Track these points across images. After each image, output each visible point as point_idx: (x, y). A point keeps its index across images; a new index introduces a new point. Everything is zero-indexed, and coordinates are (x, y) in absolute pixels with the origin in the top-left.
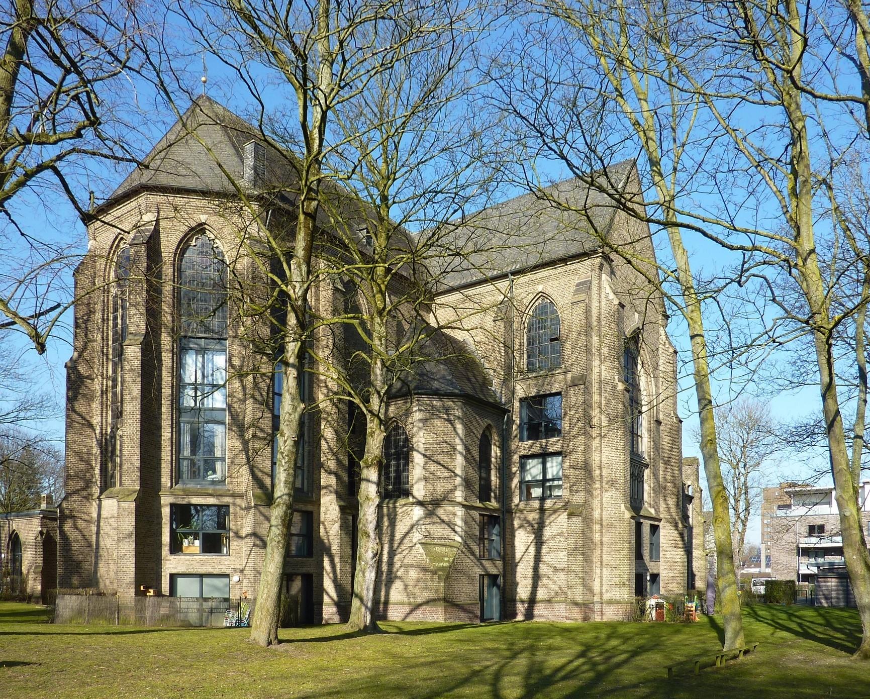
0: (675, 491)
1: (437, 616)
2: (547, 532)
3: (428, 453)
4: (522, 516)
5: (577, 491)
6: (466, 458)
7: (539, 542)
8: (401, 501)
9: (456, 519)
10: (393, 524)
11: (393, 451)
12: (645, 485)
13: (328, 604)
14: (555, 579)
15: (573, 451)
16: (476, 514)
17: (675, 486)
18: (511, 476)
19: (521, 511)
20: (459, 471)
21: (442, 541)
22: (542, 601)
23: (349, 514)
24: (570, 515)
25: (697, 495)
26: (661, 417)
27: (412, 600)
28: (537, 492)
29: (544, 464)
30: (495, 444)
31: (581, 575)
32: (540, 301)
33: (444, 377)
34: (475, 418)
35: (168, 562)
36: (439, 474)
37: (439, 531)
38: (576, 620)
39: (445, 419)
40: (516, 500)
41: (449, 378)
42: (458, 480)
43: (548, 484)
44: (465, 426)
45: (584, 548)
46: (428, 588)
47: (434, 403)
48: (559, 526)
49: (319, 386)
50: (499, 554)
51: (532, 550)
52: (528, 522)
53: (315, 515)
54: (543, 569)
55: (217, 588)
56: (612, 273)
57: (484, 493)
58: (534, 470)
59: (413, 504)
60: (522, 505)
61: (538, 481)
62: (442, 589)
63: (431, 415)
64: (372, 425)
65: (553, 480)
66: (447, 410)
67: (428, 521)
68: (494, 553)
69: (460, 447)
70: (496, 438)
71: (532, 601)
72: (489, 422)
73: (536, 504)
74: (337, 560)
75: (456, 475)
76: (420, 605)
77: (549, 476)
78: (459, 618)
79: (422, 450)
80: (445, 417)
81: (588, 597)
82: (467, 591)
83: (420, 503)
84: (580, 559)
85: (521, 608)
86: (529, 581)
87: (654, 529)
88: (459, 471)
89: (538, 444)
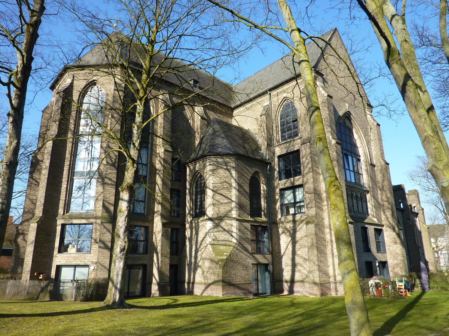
0: (390, 206)
1: (217, 292)
2: (299, 235)
3: (215, 189)
4: (284, 226)
5: (311, 208)
6: (238, 191)
7: (294, 242)
8: (201, 219)
9: (233, 228)
10: (197, 233)
11: (199, 190)
12: (368, 204)
13: (154, 284)
14: (305, 266)
15: (307, 182)
16: (248, 225)
17: (389, 203)
18: (275, 202)
19: (282, 223)
20: (234, 199)
21: (224, 243)
22: (298, 281)
23: (168, 227)
24: (307, 223)
25: (420, 212)
26: (374, 162)
27: (206, 281)
28: (292, 211)
29: (294, 193)
30: (263, 183)
31: (317, 263)
32: (286, 102)
33: (225, 146)
34: (245, 167)
35: (56, 258)
36: (222, 201)
37: (223, 236)
38: (316, 295)
39: (225, 169)
40: (279, 216)
41: (229, 146)
42: (234, 205)
43: (297, 205)
44: (238, 172)
45: (319, 246)
46: (214, 273)
47: (219, 160)
48: (303, 231)
49: (156, 156)
50: (269, 250)
51: (290, 247)
52: (287, 229)
53: (150, 228)
54: (298, 260)
55: (83, 274)
56: (324, 81)
57: (255, 211)
58: (289, 197)
59: (206, 220)
60: (283, 219)
61: (291, 203)
62: (221, 274)
63: (218, 166)
64: (129, 164)
65: (300, 202)
66: (226, 164)
67: (216, 230)
68: (266, 250)
69: (234, 185)
70: (263, 179)
71: (292, 281)
72: (257, 170)
73: (290, 218)
74: (160, 255)
75: (232, 201)
76: (210, 285)
77: (298, 200)
78: (235, 294)
79: (212, 188)
80: (225, 167)
81: (324, 278)
82: (244, 274)
83: (210, 219)
84: (315, 252)
85: (286, 286)
86: (290, 268)
87: (379, 232)
88: (234, 199)
89: (289, 181)
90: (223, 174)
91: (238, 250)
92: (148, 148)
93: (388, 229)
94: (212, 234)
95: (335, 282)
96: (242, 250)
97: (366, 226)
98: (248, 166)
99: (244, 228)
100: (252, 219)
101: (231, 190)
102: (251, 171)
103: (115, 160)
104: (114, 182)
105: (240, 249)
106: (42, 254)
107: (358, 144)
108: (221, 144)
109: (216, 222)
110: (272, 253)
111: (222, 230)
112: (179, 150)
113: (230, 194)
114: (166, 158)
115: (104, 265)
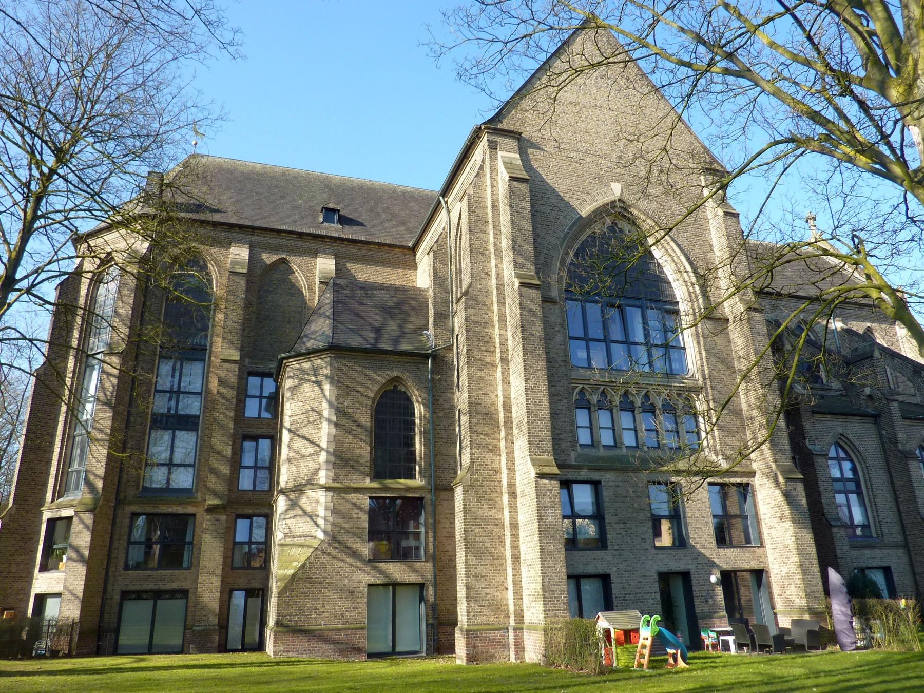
20: (324, 444)
21: (301, 540)
36: (304, 451)
39: (313, 382)
42: (323, 456)
66: (316, 371)
67: (291, 513)
75: (322, 449)
80: (313, 379)
88: (324, 444)
90: (308, 394)
91: (329, 554)
92: (204, 360)
93: (765, 481)
94: (284, 522)
95: (519, 626)
96: (339, 556)
98: (371, 368)
99: (350, 506)
100: (375, 485)
102: (380, 379)
103: (112, 393)
104: (106, 434)
105: (334, 552)
106: (11, 575)
107: (669, 271)
108: (316, 332)
109: (292, 496)
110: (434, 559)
111: (300, 512)
114: (223, 375)
115: (74, 592)
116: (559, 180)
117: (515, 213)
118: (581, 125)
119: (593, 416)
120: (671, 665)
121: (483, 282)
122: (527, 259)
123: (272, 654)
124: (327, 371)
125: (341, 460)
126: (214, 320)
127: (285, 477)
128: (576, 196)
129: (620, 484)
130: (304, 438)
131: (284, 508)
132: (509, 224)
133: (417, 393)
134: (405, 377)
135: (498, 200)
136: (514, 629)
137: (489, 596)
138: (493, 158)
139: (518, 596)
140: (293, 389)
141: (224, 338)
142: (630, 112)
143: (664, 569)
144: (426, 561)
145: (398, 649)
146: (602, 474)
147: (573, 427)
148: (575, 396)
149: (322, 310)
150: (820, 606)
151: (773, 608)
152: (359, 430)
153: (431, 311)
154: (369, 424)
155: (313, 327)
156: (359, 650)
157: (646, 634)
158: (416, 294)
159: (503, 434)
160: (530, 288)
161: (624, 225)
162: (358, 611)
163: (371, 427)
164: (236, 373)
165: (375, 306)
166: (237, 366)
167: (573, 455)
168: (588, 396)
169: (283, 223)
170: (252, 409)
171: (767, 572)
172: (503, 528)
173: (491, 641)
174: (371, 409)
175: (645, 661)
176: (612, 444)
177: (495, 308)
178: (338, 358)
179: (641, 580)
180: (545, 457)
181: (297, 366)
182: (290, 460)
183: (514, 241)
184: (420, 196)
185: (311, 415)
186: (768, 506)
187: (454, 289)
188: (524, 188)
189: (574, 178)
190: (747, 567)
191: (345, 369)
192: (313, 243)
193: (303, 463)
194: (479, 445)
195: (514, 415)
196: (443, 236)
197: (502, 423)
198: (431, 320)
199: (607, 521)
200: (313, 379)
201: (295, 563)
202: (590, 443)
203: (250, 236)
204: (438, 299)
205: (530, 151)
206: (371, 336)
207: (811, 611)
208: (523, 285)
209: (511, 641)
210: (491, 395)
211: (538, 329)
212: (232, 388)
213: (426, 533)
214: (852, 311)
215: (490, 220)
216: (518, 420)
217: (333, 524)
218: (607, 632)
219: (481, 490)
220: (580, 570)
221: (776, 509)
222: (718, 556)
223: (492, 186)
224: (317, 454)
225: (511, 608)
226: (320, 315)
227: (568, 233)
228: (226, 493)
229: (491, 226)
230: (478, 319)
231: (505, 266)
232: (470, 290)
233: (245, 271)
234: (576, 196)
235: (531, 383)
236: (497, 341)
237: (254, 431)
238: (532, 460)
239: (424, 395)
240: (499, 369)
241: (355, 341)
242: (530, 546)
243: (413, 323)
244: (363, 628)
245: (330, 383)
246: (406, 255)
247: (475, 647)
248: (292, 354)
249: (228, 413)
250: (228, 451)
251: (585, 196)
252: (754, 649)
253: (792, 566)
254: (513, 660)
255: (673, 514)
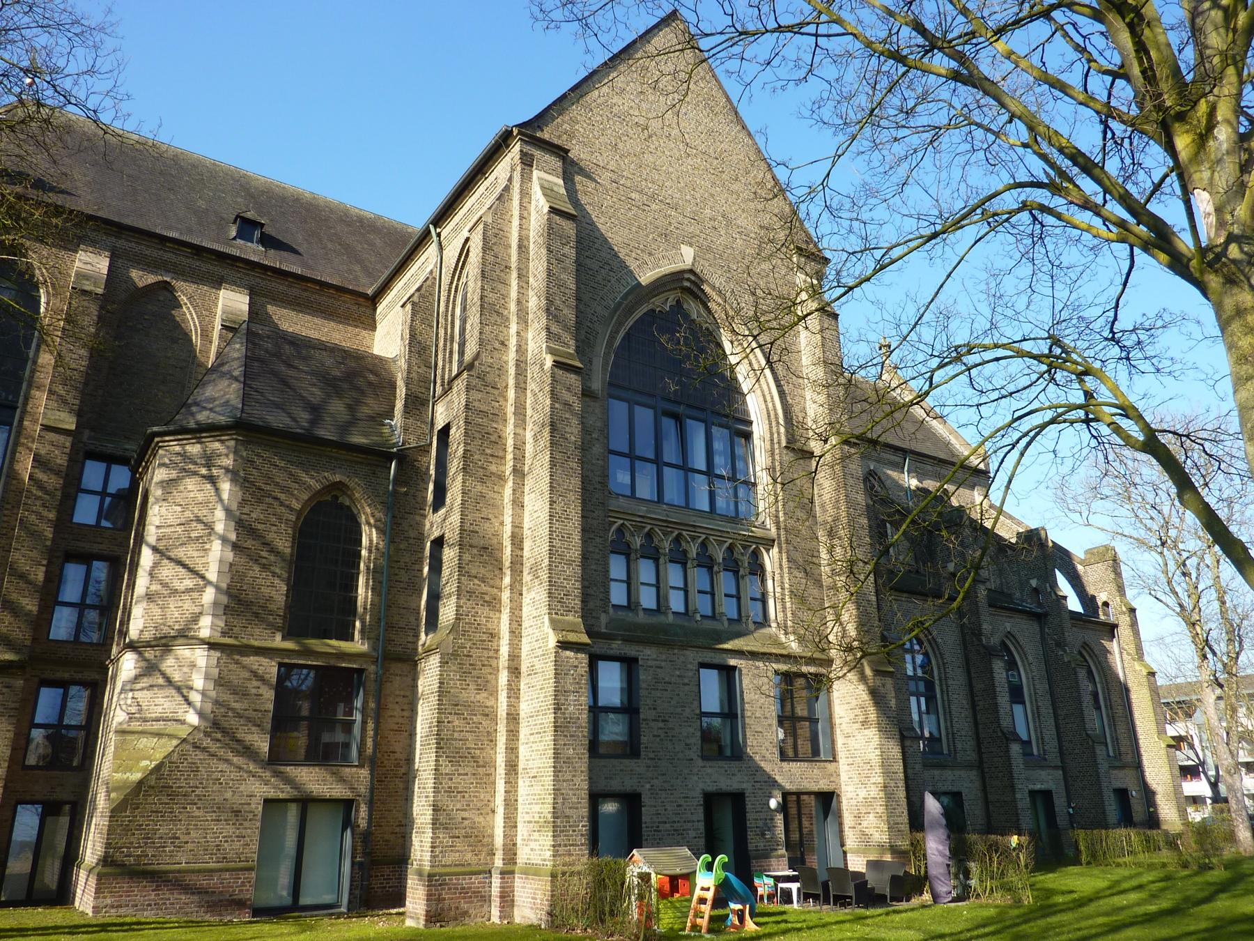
3: (161, 546)
9: (194, 676)
20: (212, 576)
21: (157, 726)
25: (1124, 621)
39: (203, 476)
42: (209, 595)
67: (145, 682)
75: (210, 583)
80: (204, 471)
88: (212, 576)
90: (192, 495)
91: (204, 749)
92: (11, 425)
94: (130, 694)
95: (509, 868)
96: (221, 753)
97: (732, 662)
98: (301, 465)
99: (247, 675)
100: (289, 645)
101: (207, 546)
102: (312, 482)
105: (214, 747)
108: (214, 399)
109: (149, 654)
110: (373, 763)
111: (161, 681)
112: (623, 478)
113: (204, 560)
114: (43, 452)
116: (615, 230)
117: (553, 261)
118: (649, 158)
119: (632, 566)
120: (733, 926)
121: (496, 355)
122: (566, 328)
123: (90, 912)
124: (228, 462)
125: (238, 603)
126: (35, 362)
127: (139, 623)
128: (634, 255)
129: (663, 664)
130: (179, 563)
131: (133, 673)
132: (544, 276)
133: (368, 510)
134: (352, 485)
135: (528, 238)
136: (501, 873)
137: (466, 822)
138: (526, 178)
139: (511, 823)
140: (168, 485)
141: (51, 392)
142: (712, 154)
143: (712, 788)
144: (361, 766)
145: (305, 900)
146: (641, 648)
147: (606, 580)
148: (611, 535)
149: (226, 368)
150: (904, 844)
151: (843, 845)
152: (272, 558)
153: (401, 391)
154: (288, 551)
155: (209, 391)
156: (240, 904)
157: (706, 882)
158: (375, 365)
159: (507, 580)
160: (567, 370)
161: (693, 308)
162: (243, 842)
163: (292, 555)
164: (68, 451)
165: (312, 373)
166: (70, 439)
167: (604, 619)
168: (628, 537)
169: (170, 228)
170: (86, 511)
171: (838, 796)
172: (495, 720)
173: (464, 891)
174: (294, 528)
175: (704, 923)
176: (655, 607)
177: (511, 394)
178: (249, 442)
179: (682, 802)
180: (570, 618)
181: (177, 449)
182: (150, 597)
183: (550, 301)
184: (384, 227)
185: (190, 533)
186: (846, 707)
187: (440, 364)
188: (569, 228)
189: (634, 229)
190: (815, 788)
191: (258, 461)
192: (217, 267)
193: (172, 603)
194: (471, 593)
195: (526, 553)
196: (429, 282)
197: (507, 563)
198: (399, 405)
199: (642, 716)
200: (204, 471)
201: (145, 763)
202: (625, 604)
203: (114, 240)
204: (414, 375)
205: (578, 178)
206: (304, 416)
207: (894, 850)
208: (557, 364)
209: (495, 889)
210: (493, 520)
211: (573, 432)
212: (57, 473)
213: (364, 722)
214: (929, 467)
215: (514, 265)
216: (532, 561)
217: (217, 702)
218: (645, 878)
219: (467, 661)
220: (602, 786)
221: (858, 712)
222: (781, 770)
223: (522, 217)
224: (201, 590)
225: (499, 841)
226: (223, 375)
227: (620, 304)
228: (28, 643)
229: (514, 275)
230: (484, 408)
231: (530, 336)
232: (476, 363)
233: (100, 291)
234: (634, 255)
235: (558, 508)
236: (510, 442)
237: (85, 546)
238: (552, 621)
239: (379, 515)
240: (510, 483)
241: (277, 420)
242: (536, 749)
243: (371, 406)
244: (250, 869)
245: (231, 480)
246: (363, 307)
247: (440, 900)
248: (172, 428)
249: (45, 513)
250: (40, 575)
251: (646, 257)
252: (827, 902)
253: (873, 787)
254: (495, 919)
255: (726, 710)
